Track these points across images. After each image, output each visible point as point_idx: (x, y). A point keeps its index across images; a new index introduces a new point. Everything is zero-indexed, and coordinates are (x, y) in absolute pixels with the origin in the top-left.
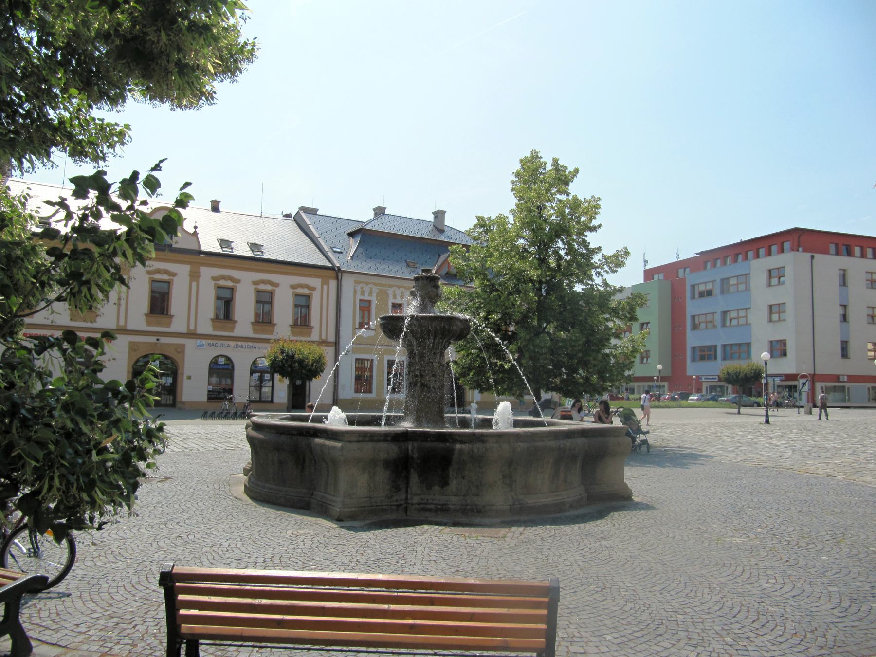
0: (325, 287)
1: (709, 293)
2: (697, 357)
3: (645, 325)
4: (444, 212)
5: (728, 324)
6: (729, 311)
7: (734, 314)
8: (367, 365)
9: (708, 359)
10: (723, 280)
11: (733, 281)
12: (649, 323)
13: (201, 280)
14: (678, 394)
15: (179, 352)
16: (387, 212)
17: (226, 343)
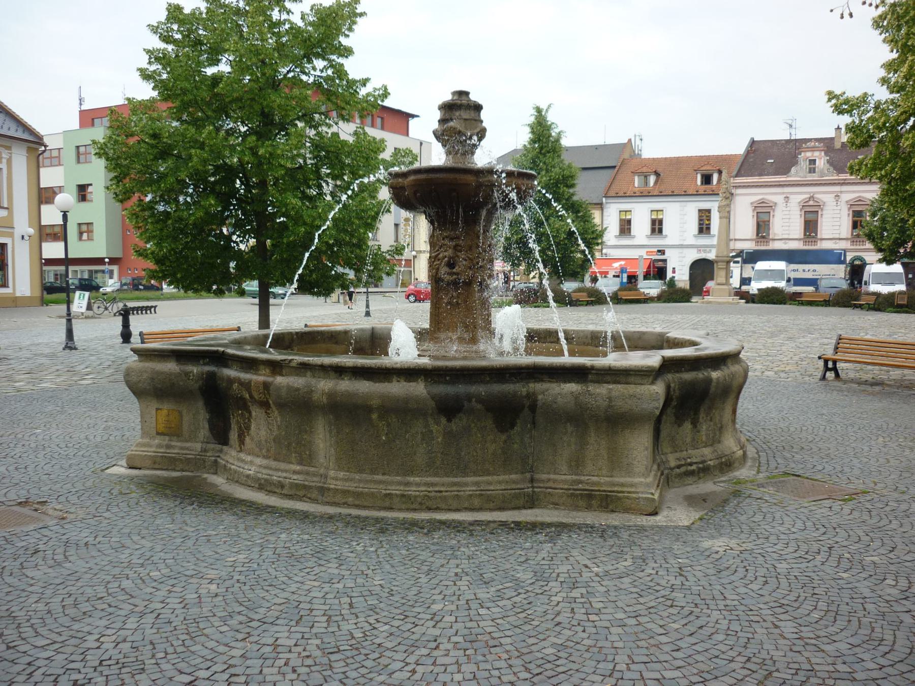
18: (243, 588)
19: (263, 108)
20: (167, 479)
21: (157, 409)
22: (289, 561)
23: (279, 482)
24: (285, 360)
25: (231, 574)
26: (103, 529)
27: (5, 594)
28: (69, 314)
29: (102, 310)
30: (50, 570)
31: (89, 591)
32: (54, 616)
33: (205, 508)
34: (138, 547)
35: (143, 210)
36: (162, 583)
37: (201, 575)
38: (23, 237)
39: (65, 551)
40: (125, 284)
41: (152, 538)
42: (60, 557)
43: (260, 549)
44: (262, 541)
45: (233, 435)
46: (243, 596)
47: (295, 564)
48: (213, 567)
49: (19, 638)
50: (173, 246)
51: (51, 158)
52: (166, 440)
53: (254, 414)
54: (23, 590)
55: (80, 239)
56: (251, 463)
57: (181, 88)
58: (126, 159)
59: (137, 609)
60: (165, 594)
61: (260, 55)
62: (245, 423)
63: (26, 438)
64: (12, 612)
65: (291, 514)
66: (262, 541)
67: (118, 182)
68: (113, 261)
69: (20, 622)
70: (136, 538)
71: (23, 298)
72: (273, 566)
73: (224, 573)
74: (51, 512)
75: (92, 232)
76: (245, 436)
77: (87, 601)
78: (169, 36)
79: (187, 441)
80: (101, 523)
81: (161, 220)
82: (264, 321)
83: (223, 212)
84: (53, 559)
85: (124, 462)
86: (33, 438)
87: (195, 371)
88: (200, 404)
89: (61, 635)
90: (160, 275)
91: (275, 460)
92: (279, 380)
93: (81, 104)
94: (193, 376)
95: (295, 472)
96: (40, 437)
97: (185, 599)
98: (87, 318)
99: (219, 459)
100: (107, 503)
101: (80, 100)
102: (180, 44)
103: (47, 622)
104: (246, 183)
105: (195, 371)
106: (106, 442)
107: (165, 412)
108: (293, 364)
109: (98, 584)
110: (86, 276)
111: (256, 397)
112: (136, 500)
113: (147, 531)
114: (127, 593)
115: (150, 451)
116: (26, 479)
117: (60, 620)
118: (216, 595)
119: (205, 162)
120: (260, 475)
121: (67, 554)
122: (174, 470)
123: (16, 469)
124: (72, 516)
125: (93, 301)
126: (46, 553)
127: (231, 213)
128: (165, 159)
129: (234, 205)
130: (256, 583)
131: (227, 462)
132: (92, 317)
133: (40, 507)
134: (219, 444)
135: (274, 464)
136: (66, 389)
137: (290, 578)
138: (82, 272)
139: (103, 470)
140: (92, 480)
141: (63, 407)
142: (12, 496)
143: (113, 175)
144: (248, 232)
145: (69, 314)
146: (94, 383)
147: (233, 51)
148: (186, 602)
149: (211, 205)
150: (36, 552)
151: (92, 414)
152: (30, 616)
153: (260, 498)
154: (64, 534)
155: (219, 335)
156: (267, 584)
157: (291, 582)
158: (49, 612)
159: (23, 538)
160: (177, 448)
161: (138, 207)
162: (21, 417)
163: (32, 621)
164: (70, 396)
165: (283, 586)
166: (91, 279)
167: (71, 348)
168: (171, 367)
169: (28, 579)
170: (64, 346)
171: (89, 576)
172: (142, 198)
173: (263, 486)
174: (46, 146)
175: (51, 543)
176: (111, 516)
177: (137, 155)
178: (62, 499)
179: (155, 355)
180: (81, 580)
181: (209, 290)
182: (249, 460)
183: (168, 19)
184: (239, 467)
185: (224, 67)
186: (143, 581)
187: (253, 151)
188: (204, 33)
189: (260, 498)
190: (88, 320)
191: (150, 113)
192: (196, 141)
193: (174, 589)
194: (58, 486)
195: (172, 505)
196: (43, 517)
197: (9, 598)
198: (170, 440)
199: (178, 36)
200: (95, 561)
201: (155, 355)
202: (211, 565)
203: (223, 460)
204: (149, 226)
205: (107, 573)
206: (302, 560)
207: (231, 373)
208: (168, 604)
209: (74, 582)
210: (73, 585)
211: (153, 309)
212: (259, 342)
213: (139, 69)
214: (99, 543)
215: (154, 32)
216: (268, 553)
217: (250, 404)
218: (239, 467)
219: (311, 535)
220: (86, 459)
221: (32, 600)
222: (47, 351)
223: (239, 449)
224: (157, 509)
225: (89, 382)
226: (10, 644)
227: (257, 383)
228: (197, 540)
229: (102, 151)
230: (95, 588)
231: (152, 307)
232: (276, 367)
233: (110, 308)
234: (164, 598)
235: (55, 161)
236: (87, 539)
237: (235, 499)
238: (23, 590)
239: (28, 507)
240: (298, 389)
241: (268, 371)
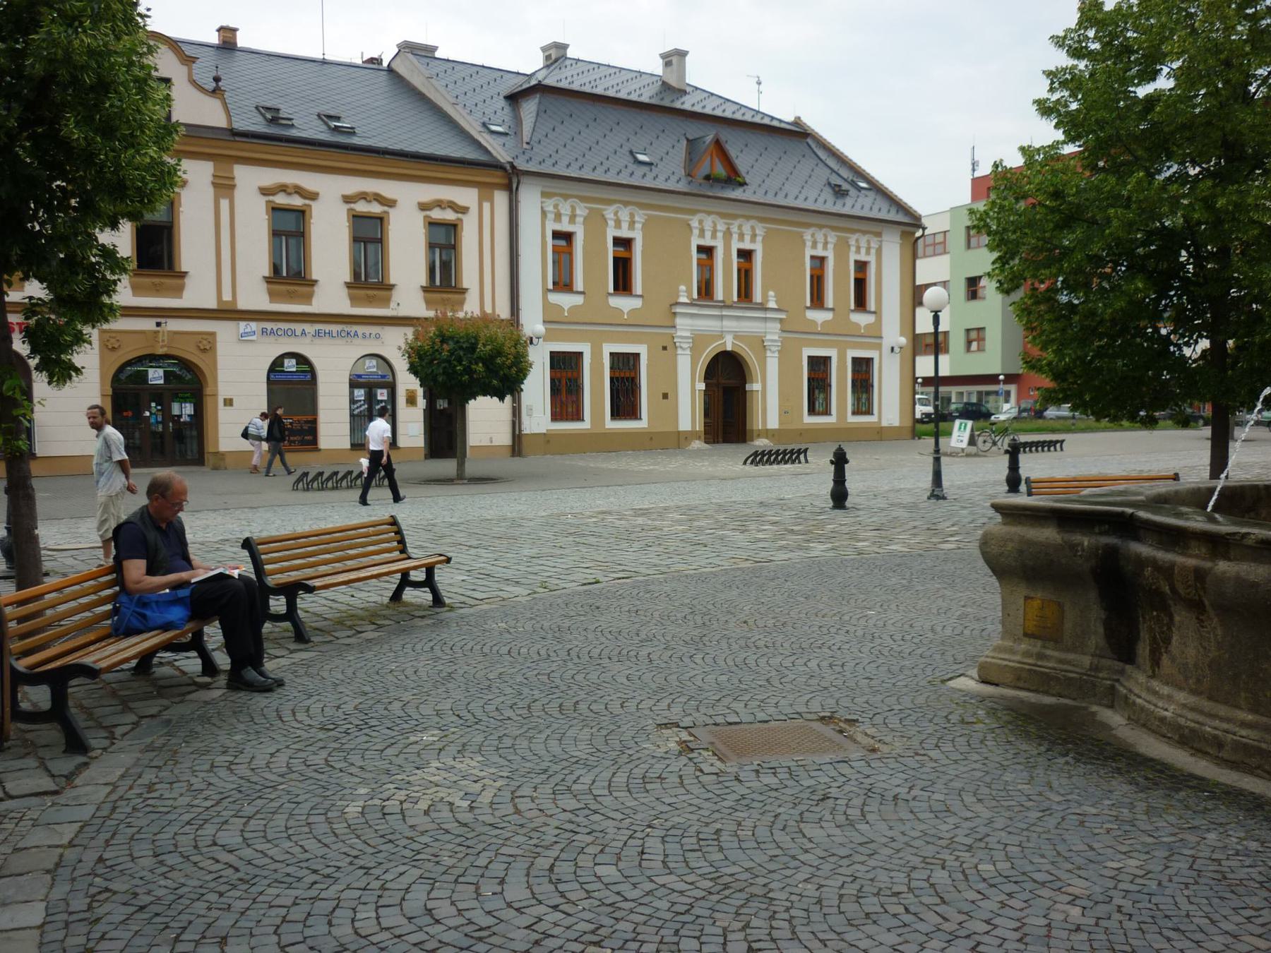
0: (486, 206)
4: (682, 54)
13: (238, 193)
15: (204, 350)
17: (298, 327)
18: (1127, 924)
19: (1225, 135)
20: (1033, 706)
21: (1027, 598)
22: (1216, 888)
23: (1215, 737)
24: (1234, 534)
25: (1111, 893)
26: (923, 777)
27: (767, 858)
28: (937, 451)
29: (989, 445)
30: (838, 832)
31: (883, 877)
32: (825, 910)
33: (1085, 763)
34: (969, 815)
35: (1037, 303)
36: (994, 886)
37: (1059, 884)
38: (892, 349)
39: (864, 804)
40: (1025, 410)
41: (994, 803)
42: (854, 813)
43: (1167, 854)
44: (1172, 839)
45: (1143, 650)
46: (1122, 939)
47: (1228, 895)
48: (1081, 873)
49: (768, 938)
50: (1079, 353)
51: (934, 244)
52: (1037, 646)
53: (1177, 618)
54: (794, 857)
55: (968, 349)
56: (1169, 698)
57: (1096, 120)
58: (1014, 232)
59: (947, 926)
60: (995, 906)
61: (1221, 52)
62: (1163, 633)
63: (854, 621)
64: (771, 890)
65: (1232, 796)
66: (1172, 839)
67: (1004, 265)
68: (1010, 378)
69: (776, 909)
70: (969, 799)
71: (891, 428)
72: (1186, 892)
73: (1098, 889)
74: (859, 737)
75: (984, 339)
76: (1161, 654)
77: (878, 894)
78: (1082, 48)
79: (1068, 650)
80: (923, 766)
81: (1064, 316)
82: (1219, 461)
83: (1158, 300)
84: (845, 813)
85: (974, 672)
86: (862, 622)
87: (1086, 543)
88: (1093, 595)
89: (825, 946)
90: (1061, 396)
91: (1210, 698)
92: (1222, 566)
93: (974, 170)
94: (1083, 550)
95: (1244, 724)
96: (871, 622)
97: (1024, 924)
98: (968, 455)
99: (1117, 685)
100: (938, 735)
101: (973, 164)
102: (1098, 57)
103: (812, 919)
104: (1197, 257)
105: (1086, 543)
106: (957, 637)
107: (1037, 603)
108: (1249, 542)
109: (897, 868)
110: (974, 400)
111: (1182, 590)
112: (980, 735)
113: (987, 791)
114: (937, 894)
115: (1013, 660)
116: (839, 683)
117: (831, 920)
118: (1078, 929)
119: (1130, 226)
120: (1182, 721)
121: (866, 808)
122: (1046, 693)
123: (831, 666)
124: (885, 749)
125: (977, 433)
126: (838, 802)
127: (1172, 301)
128: (1071, 227)
129: (1177, 289)
130: (1150, 920)
131: (1131, 691)
132: (976, 455)
133: (847, 727)
134: (1119, 661)
135: (1207, 705)
136: (920, 555)
137: (1213, 922)
138: (970, 394)
139: (943, 682)
140: (926, 695)
141: (910, 581)
142: (815, 706)
143: (996, 255)
144: (1198, 328)
145: (937, 451)
146: (959, 548)
147: (1177, 53)
148: (1026, 930)
149: (1137, 289)
150: (825, 798)
151: (948, 593)
152: (792, 902)
153: (1180, 758)
154: (868, 776)
155: (1132, 486)
156: (1170, 925)
157: (1215, 930)
158: (819, 902)
159: (813, 774)
160: (1054, 661)
161: (1030, 298)
162: (854, 591)
163: (793, 912)
164: (923, 566)
165: (1199, 936)
166: (979, 403)
167: (938, 497)
168: (1048, 534)
169: (805, 841)
170: (929, 494)
171: (888, 851)
172: (1037, 285)
173: (1187, 739)
174: (924, 229)
175: (847, 788)
176: (941, 756)
177: (1030, 224)
178: (879, 720)
179: (1026, 516)
180: (876, 856)
181: (1133, 418)
182: (1166, 692)
183: (1080, 23)
184: (1149, 702)
185: (1164, 83)
186: (966, 876)
187: (1208, 203)
188: (1135, 35)
189: (1180, 758)
190: (969, 459)
191: (1052, 164)
192: (1120, 196)
193: (1012, 902)
194: (879, 697)
195: (1036, 752)
196: (847, 744)
197: (772, 866)
198: (1044, 647)
199: (1095, 46)
200: (903, 829)
201: (1026, 516)
202: (1079, 868)
203: (1124, 687)
204: (1046, 326)
205: (915, 851)
206: (1241, 890)
207: (1143, 549)
208: (996, 927)
209: (866, 858)
210: (862, 863)
211: (1058, 445)
212: (1198, 498)
213: (1035, 102)
214: (914, 799)
215: (1060, 46)
216: (1181, 865)
217: (1171, 602)
218: (1149, 702)
219: (1262, 843)
220: (924, 661)
221: (801, 876)
222: (907, 499)
223: (1150, 673)
224: (1010, 756)
225: (953, 546)
226: (753, 944)
227: (1184, 568)
228: (1063, 819)
229: (982, 223)
230: (892, 874)
231: (1057, 442)
232: (1218, 545)
233: (999, 443)
234: (991, 915)
235: (939, 249)
236: (898, 790)
237: (1138, 754)
238: (794, 857)
239: (832, 726)
240: (1254, 585)
241: (1204, 550)
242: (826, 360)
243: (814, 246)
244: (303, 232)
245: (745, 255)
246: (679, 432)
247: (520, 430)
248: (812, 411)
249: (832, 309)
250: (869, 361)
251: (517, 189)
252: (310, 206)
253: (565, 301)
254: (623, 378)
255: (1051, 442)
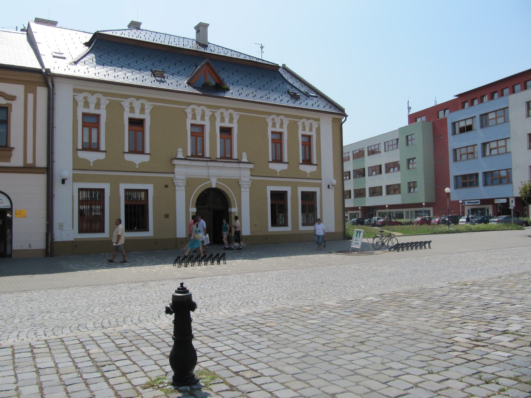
0: (30, 96)
1: (469, 128)
2: (460, 184)
3: (411, 161)
4: (206, 26)
5: (488, 153)
6: (489, 143)
7: (493, 145)
8: (84, 195)
9: (469, 186)
10: (481, 116)
11: (491, 116)
12: (415, 158)
14: (449, 217)
16: (142, 27)
38: (329, 187)
211: (427, 245)
231: (426, 242)
242: (284, 194)
243: (304, 129)
244: (7, 120)
245: (226, 131)
246: (177, 239)
247: (52, 239)
248: (274, 223)
249: (287, 163)
250: (314, 194)
251: (53, 85)
252: (11, 105)
253: (92, 157)
254: (135, 205)
255: (421, 243)
